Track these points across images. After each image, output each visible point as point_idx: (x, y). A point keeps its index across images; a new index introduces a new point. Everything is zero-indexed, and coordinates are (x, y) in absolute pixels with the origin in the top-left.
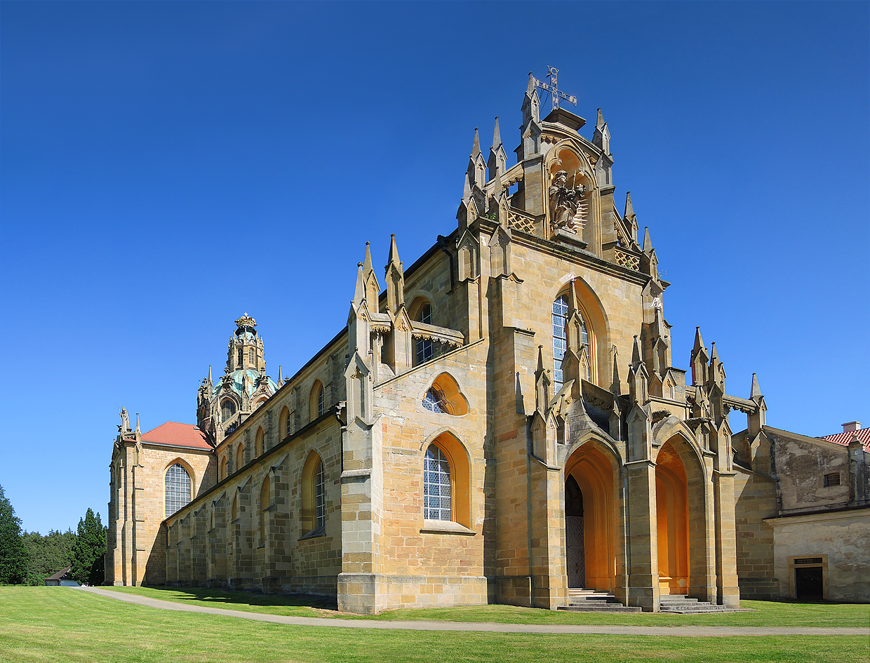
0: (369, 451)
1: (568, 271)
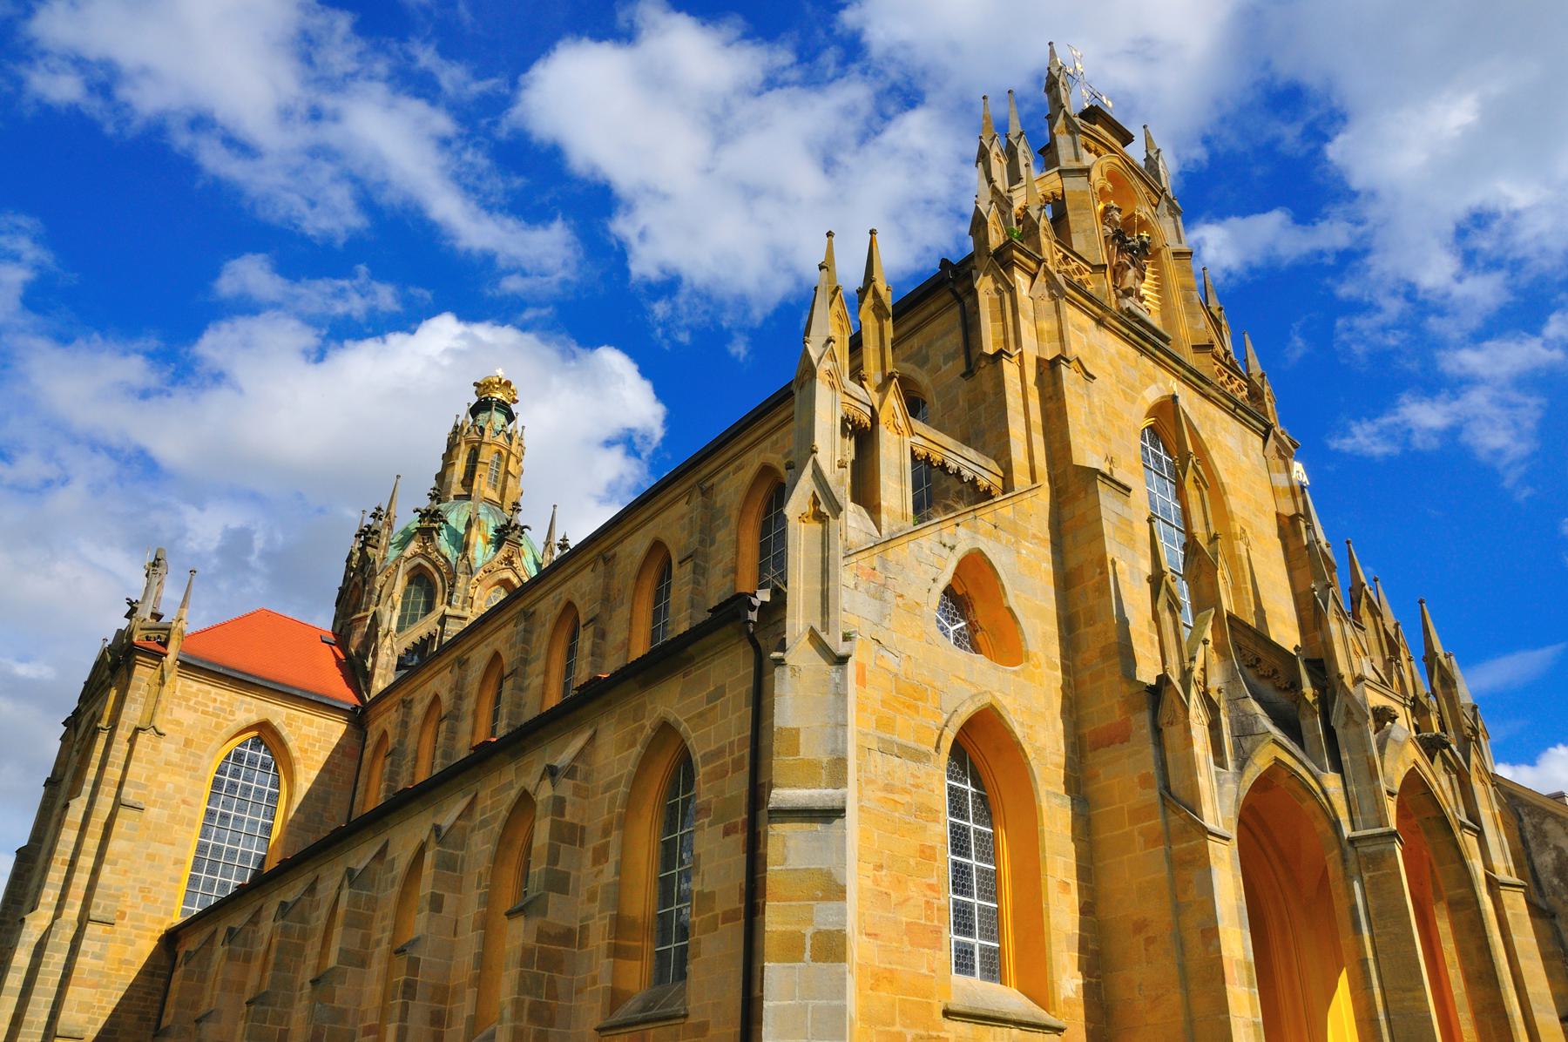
0: (840, 732)
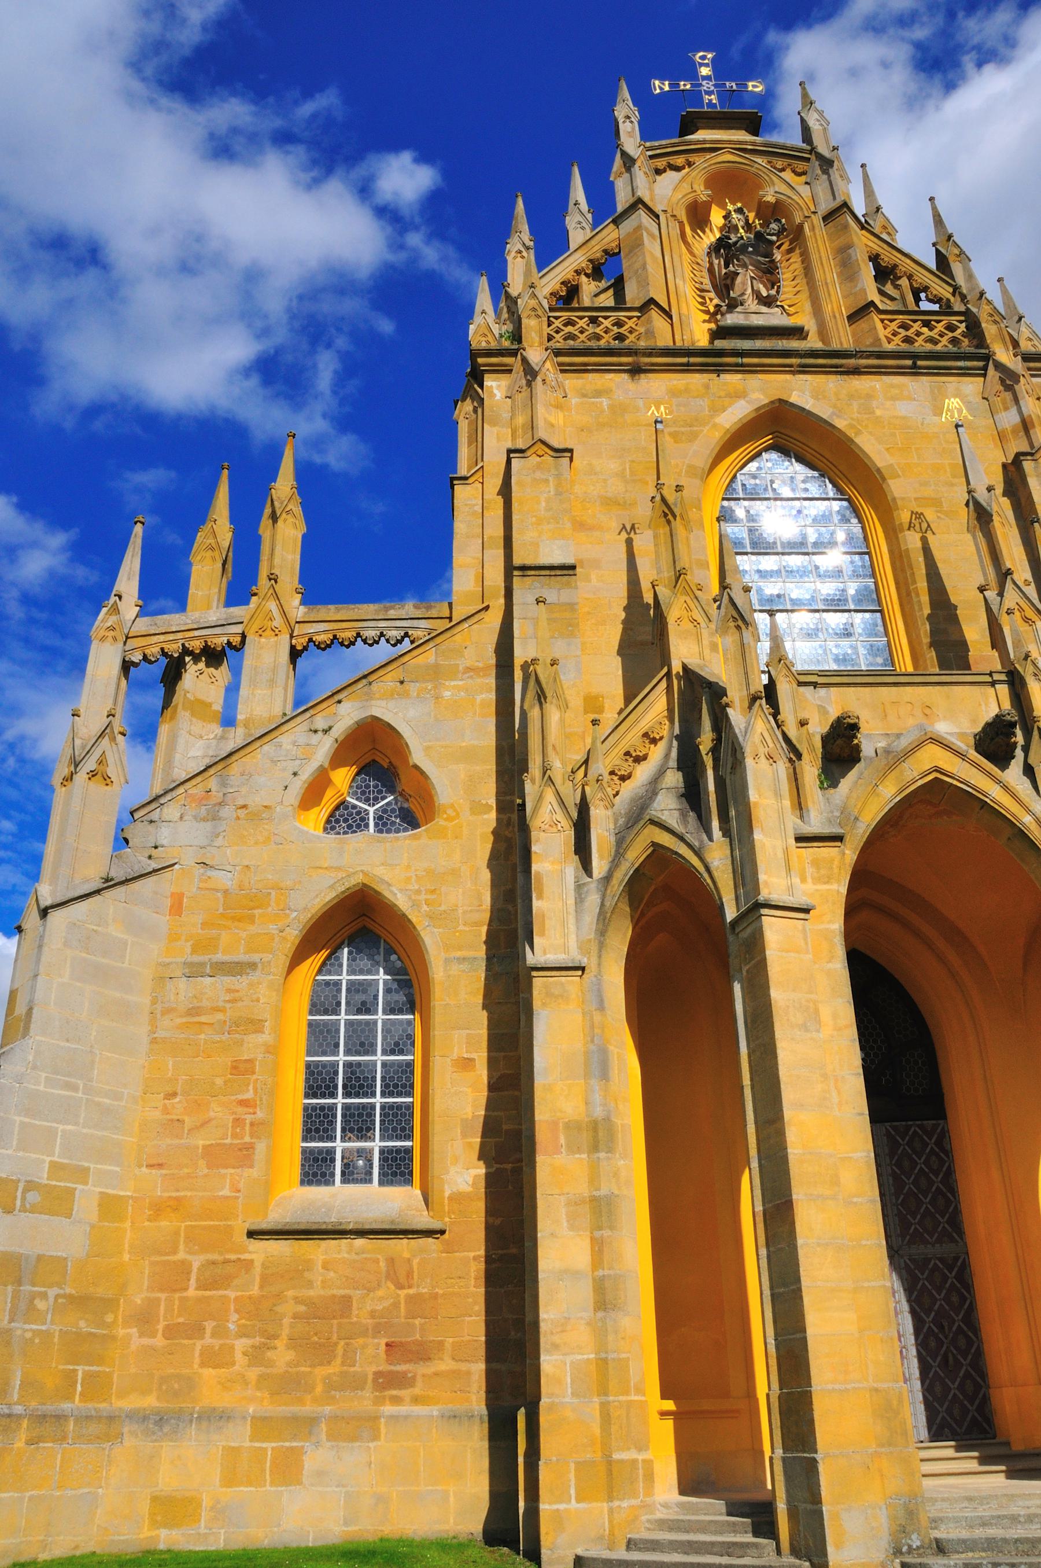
1: (740, 395)
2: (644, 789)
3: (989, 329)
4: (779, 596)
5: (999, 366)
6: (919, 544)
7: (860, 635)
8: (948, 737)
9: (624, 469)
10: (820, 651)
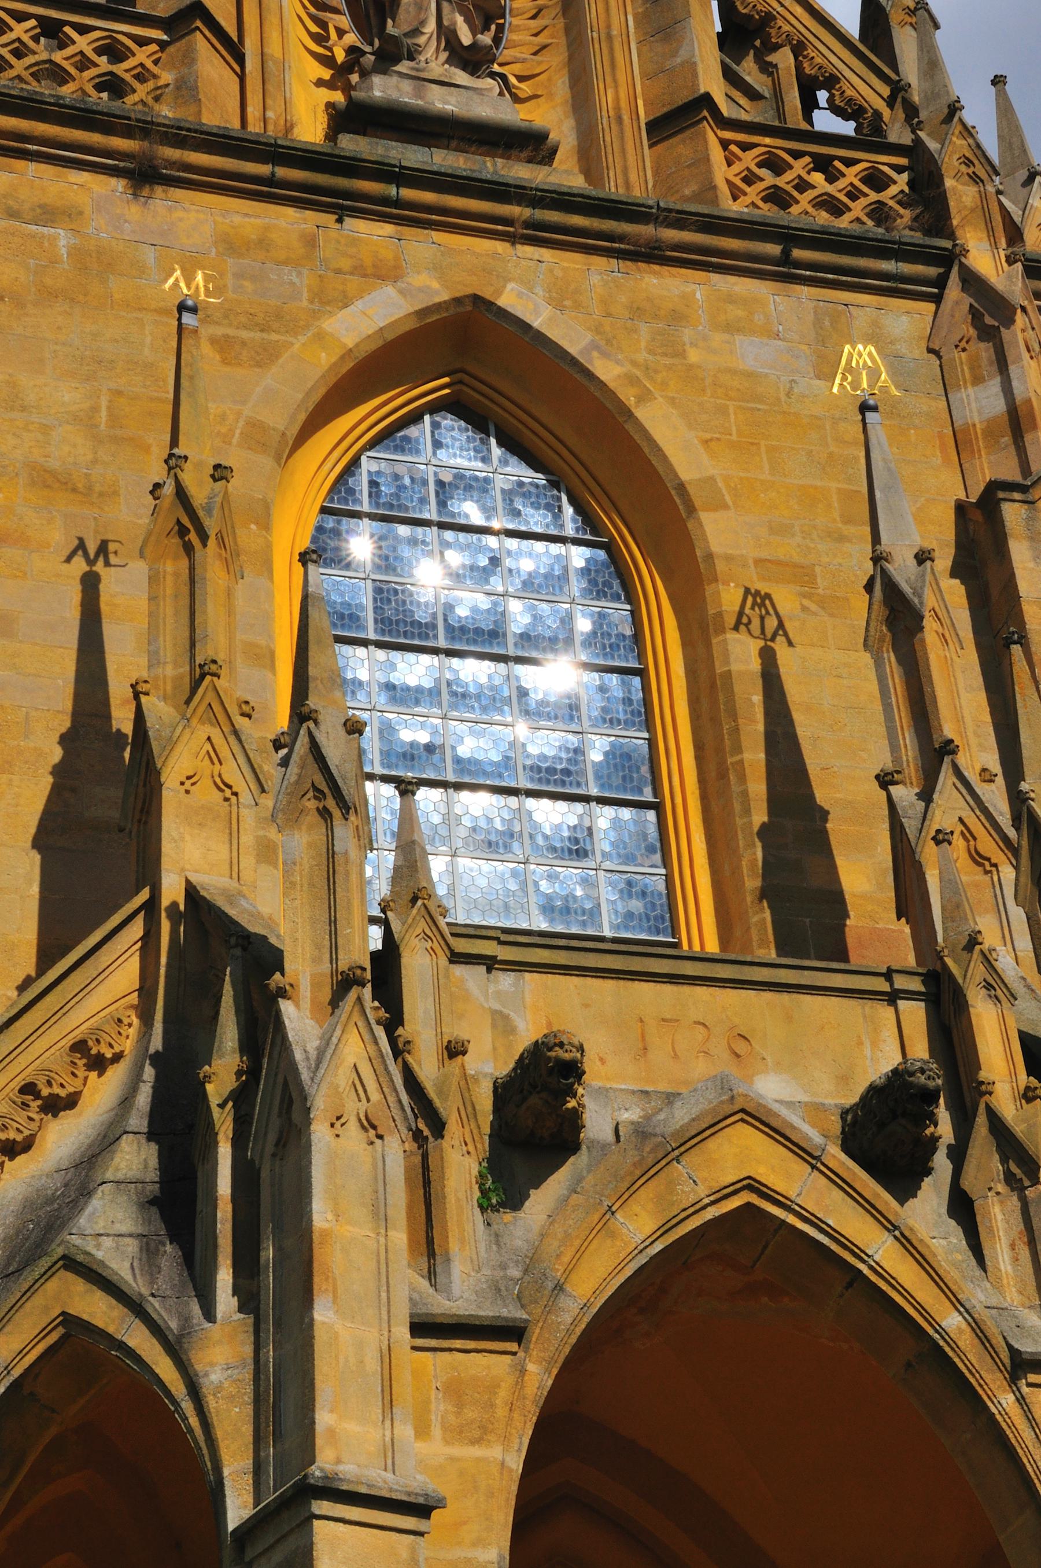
2: (59, 1180)
3: (960, 194)
4: (430, 748)
5: (972, 282)
6: (755, 665)
7: (604, 855)
8: (784, 1112)
9: (95, 409)
10: (513, 886)
